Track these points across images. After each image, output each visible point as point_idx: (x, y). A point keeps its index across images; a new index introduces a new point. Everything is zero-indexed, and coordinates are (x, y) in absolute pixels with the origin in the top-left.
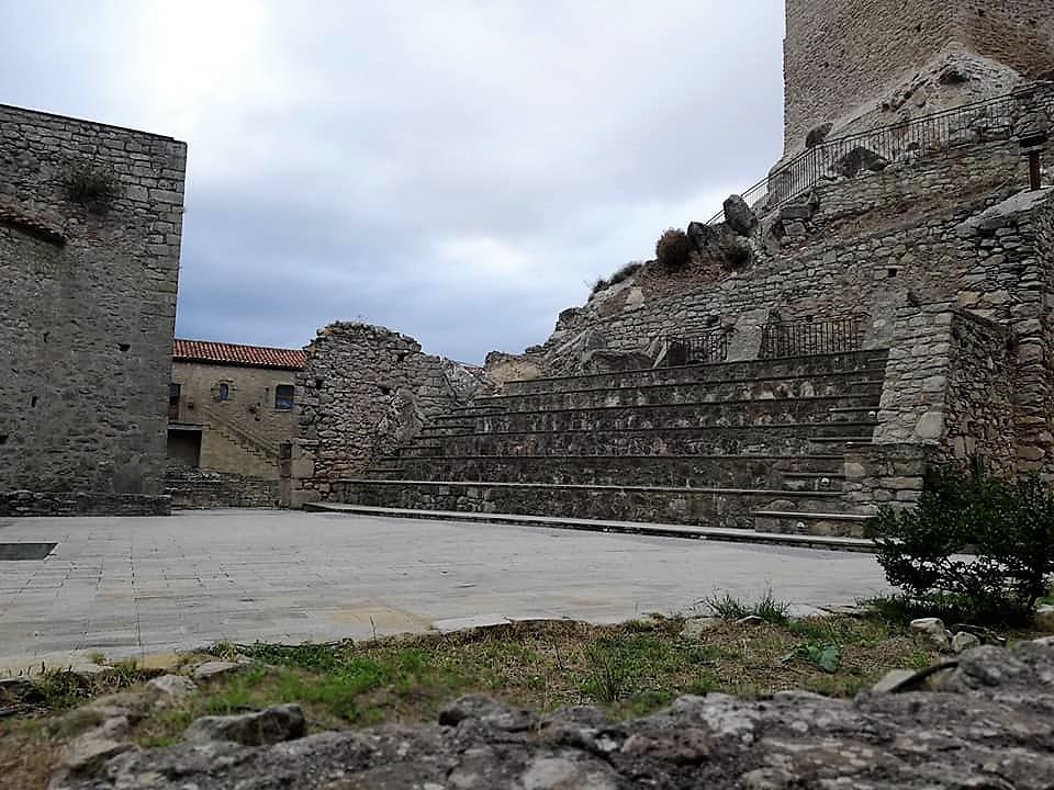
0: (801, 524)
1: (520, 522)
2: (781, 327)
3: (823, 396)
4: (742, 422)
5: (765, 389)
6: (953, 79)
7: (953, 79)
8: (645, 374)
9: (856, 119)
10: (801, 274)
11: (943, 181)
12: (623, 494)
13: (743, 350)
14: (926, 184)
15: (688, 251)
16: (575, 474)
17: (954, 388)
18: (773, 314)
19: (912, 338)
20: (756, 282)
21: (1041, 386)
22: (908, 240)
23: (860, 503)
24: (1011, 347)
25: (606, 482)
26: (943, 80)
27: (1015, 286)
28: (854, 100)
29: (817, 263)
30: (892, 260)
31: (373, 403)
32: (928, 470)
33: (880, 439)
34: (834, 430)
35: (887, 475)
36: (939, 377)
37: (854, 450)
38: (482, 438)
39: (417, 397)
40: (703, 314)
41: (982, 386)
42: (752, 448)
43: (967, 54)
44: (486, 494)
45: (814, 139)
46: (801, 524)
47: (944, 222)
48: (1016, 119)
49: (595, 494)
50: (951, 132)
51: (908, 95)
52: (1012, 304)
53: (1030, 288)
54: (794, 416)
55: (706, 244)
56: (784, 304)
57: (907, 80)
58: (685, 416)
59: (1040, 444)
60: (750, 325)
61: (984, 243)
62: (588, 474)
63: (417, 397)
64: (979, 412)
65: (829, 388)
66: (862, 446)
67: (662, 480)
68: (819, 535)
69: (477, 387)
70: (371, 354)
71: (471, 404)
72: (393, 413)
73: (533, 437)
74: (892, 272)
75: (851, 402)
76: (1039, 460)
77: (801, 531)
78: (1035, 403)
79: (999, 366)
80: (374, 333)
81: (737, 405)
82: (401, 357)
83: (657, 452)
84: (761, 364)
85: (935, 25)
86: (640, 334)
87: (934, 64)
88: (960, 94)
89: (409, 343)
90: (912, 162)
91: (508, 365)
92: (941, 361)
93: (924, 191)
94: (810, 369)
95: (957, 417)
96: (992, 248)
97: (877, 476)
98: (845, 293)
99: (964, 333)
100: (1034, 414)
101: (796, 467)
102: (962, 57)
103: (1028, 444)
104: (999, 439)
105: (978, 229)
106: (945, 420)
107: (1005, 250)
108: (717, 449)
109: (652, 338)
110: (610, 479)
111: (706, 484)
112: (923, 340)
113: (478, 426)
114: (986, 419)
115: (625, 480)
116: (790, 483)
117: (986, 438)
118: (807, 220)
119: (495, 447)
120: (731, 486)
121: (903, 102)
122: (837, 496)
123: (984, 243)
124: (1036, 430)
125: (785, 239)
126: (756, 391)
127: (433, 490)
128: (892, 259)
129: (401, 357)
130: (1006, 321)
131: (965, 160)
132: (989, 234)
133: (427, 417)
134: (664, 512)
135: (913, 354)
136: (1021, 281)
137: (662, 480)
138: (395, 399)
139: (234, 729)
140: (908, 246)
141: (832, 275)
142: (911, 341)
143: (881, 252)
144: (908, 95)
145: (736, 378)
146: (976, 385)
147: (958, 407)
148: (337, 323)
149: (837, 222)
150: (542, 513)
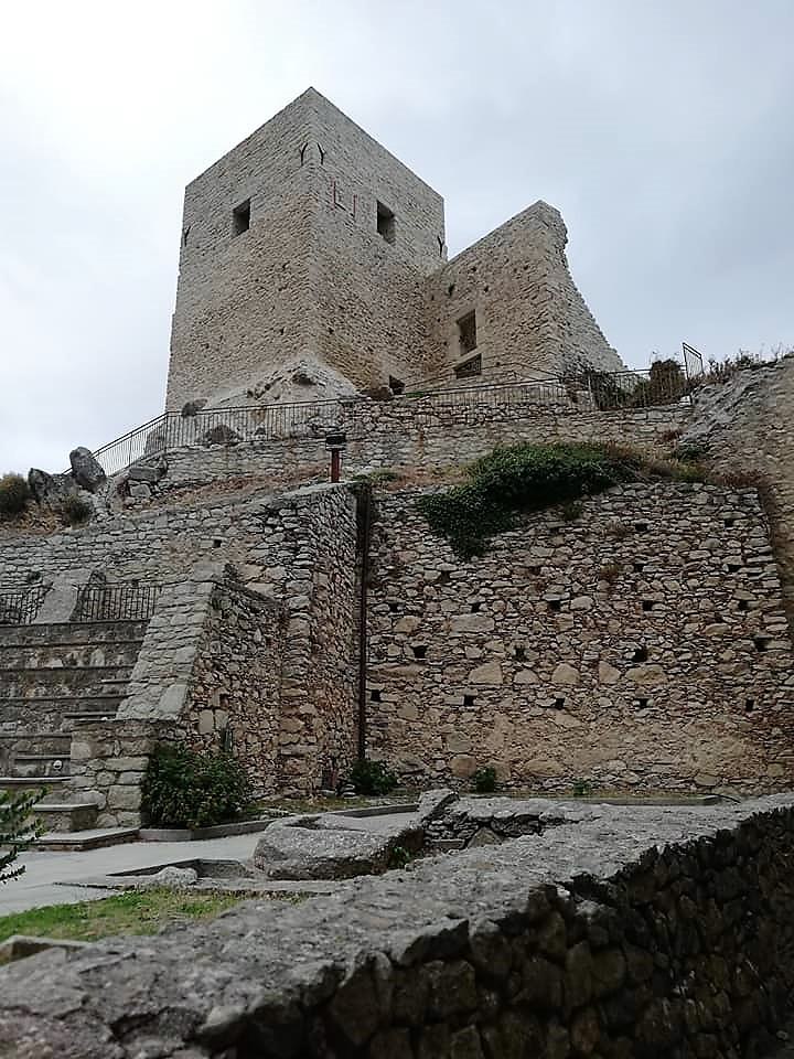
2: (105, 589)
3: (113, 664)
4: (12, 693)
5: (55, 656)
6: (303, 381)
7: (303, 381)
9: (226, 398)
10: (131, 537)
11: (277, 466)
13: (57, 610)
15: (25, 498)
17: (204, 659)
18: (95, 575)
19: (174, 606)
20: (85, 540)
21: (305, 659)
22: (234, 515)
23: (83, 789)
24: (283, 621)
27: (290, 563)
28: (227, 382)
29: (148, 526)
32: (157, 748)
35: (113, 755)
36: (190, 648)
37: (84, 727)
41: (242, 658)
43: (316, 362)
45: (190, 411)
48: (342, 422)
50: (293, 424)
51: (268, 387)
52: (288, 580)
53: (303, 567)
54: (70, 688)
57: (267, 375)
59: (300, 716)
60: (67, 586)
64: (237, 684)
65: (120, 657)
66: (93, 722)
74: (218, 543)
76: (299, 732)
78: (297, 676)
79: (268, 640)
85: (294, 332)
87: (290, 365)
88: (308, 394)
90: (256, 444)
92: (195, 631)
93: (260, 472)
94: (112, 636)
95: (206, 689)
96: (276, 526)
97: (103, 757)
99: (227, 604)
100: (296, 687)
101: (37, 748)
102: (313, 365)
103: (289, 716)
104: (260, 712)
106: (189, 693)
107: (285, 529)
112: (183, 609)
114: (244, 691)
116: (20, 768)
117: (243, 711)
118: (154, 483)
121: (263, 392)
122: (59, 782)
124: (297, 703)
125: (129, 500)
126: (44, 658)
130: (281, 596)
131: (295, 450)
132: (273, 513)
135: (172, 623)
136: (296, 559)
139: (422, 941)
140: (233, 519)
141: (162, 540)
142: (172, 609)
143: (208, 523)
144: (268, 387)
145: (33, 643)
146: (235, 657)
147: (209, 677)
149: (182, 490)
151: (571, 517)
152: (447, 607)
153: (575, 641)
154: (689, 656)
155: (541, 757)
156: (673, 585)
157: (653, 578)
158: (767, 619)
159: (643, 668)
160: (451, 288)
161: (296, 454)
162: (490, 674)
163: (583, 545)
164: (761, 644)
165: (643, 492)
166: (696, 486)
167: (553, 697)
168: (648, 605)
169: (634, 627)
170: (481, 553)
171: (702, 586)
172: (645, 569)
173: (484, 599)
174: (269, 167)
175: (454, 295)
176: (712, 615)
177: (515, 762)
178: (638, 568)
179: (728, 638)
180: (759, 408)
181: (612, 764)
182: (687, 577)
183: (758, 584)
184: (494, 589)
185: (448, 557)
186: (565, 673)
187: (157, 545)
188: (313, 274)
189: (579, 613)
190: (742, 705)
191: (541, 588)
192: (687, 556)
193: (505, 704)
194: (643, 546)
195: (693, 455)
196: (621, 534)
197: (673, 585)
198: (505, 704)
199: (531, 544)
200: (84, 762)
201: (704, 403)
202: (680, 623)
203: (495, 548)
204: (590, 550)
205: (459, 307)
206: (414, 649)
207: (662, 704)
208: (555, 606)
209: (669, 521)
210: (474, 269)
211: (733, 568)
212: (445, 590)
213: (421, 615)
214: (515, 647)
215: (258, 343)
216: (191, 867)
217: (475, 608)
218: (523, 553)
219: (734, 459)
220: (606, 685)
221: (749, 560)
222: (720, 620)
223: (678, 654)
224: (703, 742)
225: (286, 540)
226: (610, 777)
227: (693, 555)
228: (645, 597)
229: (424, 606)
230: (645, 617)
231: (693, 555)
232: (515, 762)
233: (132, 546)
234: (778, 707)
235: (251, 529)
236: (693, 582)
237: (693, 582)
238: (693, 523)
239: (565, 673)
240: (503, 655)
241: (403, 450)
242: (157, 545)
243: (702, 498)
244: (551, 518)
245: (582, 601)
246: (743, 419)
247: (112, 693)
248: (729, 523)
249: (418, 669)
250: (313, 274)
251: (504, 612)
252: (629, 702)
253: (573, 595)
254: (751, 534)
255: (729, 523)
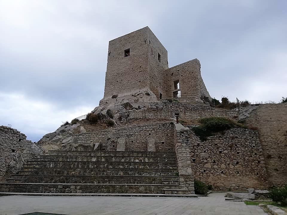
0: (176, 192)
1: (21, 195)
8: (99, 152)
12: (126, 186)
13: (121, 148)
14: (151, 116)
16: (102, 181)
20: (121, 131)
25: (112, 183)
26: (146, 94)
30: (150, 131)
31: (9, 155)
33: (181, 173)
34: (163, 170)
35: (188, 181)
38: (58, 169)
39: (23, 154)
40: (106, 137)
42: (145, 174)
44: (78, 187)
46: (176, 192)
47: (160, 126)
49: (118, 186)
51: (138, 95)
55: (103, 119)
56: (127, 137)
57: (137, 91)
58: (121, 165)
60: (122, 141)
61: (182, 134)
62: (106, 181)
63: (23, 154)
67: (129, 182)
68: (179, 194)
69: (41, 151)
70: (11, 138)
71: (39, 157)
72: (16, 159)
73: (79, 169)
75: (161, 164)
77: (176, 193)
80: (13, 131)
81: (129, 163)
82: (20, 140)
83: (120, 175)
84: (131, 152)
86: (88, 140)
89: (23, 135)
91: (48, 145)
94: (142, 155)
96: (183, 135)
97: (186, 181)
98: (140, 137)
105: (181, 131)
108: (136, 174)
109: (91, 142)
110: (113, 182)
111: (140, 183)
113: (48, 165)
115: (118, 182)
119: (63, 172)
120: (147, 183)
123: (182, 134)
125: (122, 121)
126: (134, 159)
127: (55, 186)
128: (150, 131)
129: (20, 140)
133: (25, 161)
134: (138, 191)
137: (129, 182)
138: (17, 154)
140: (153, 129)
143: (148, 129)
144: (138, 95)
148: (3, 126)
150: (99, 192)
151: (223, 134)
152: (199, 151)
153: (225, 160)
154: (246, 164)
155: (219, 183)
156: (243, 149)
157: (239, 148)
158: (260, 157)
159: (238, 166)
160: (173, 74)
161: (158, 114)
162: (209, 166)
163: (226, 140)
164: (259, 162)
165: (237, 130)
166: (246, 130)
167: (221, 171)
168: (238, 153)
169: (236, 157)
170: (206, 140)
171: (248, 150)
172: (238, 146)
173: (206, 150)
174: (135, 42)
175: (173, 76)
176: (250, 156)
177: (214, 184)
178: (236, 145)
179: (253, 161)
180: (256, 114)
181: (233, 185)
182: (245, 148)
183: (258, 150)
184: (208, 148)
185: (199, 141)
186: (223, 166)
187: (137, 133)
188: (148, 70)
189: (225, 154)
190: (256, 174)
191: (218, 148)
192: (245, 144)
193: (212, 172)
194: (237, 141)
195: (242, 122)
196: (233, 138)
197: (243, 149)
198: (212, 172)
199: (216, 139)
200: (183, 182)
201: (241, 111)
202: (244, 157)
203: (208, 139)
204: (227, 141)
205: (174, 78)
206: (193, 160)
207: (242, 173)
208: (220, 152)
209: (241, 136)
210: (179, 71)
211: (254, 146)
212: (199, 148)
213: (194, 153)
214: (213, 160)
215: (133, 83)
216: (270, 198)
217: (205, 152)
218: (214, 141)
219: (251, 124)
220: (231, 169)
221: (257, 145)
222: (251, 157)
223: (244, 163)
224: (250, 181)
225: (185, 138)
226: (233, 187)
227: (246, 143)
228: (238, 151)
229: (194, 151)
230: (238, 155)
231: (246, 143)
232: (214, 184)
233: (131, 133)
234: (263, 174)
235: (178, 135)
236: (246, 149)
237: (246, 149)
238: (246, 137)
239: (223, 166)
240: (211, 162)
241: (181, 115)
242: (137, 133)
243: (248, 132)
244: (219, 134)
245: (226, 151)
246: (252, 116)
247: (162, 168)
248: (253, 137)
249: (194, 164)
250: (148, 70)
251: (211, 153)
252: (236, 172)
253: (224, 150)
254: (257, 140)
255: (253, 137)
